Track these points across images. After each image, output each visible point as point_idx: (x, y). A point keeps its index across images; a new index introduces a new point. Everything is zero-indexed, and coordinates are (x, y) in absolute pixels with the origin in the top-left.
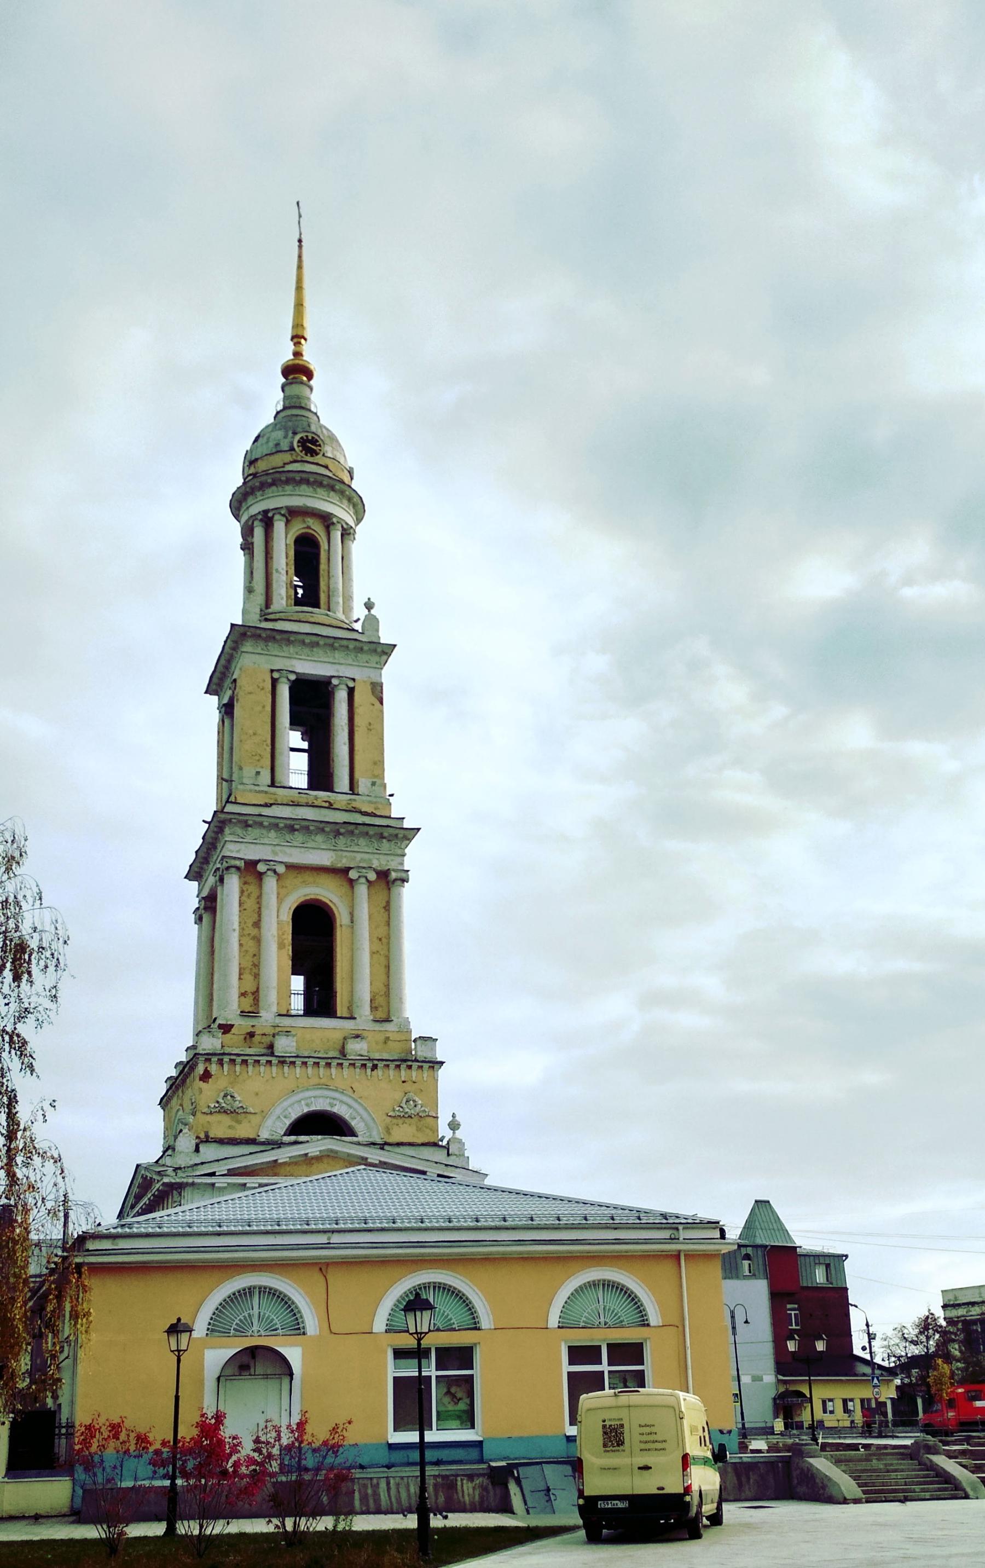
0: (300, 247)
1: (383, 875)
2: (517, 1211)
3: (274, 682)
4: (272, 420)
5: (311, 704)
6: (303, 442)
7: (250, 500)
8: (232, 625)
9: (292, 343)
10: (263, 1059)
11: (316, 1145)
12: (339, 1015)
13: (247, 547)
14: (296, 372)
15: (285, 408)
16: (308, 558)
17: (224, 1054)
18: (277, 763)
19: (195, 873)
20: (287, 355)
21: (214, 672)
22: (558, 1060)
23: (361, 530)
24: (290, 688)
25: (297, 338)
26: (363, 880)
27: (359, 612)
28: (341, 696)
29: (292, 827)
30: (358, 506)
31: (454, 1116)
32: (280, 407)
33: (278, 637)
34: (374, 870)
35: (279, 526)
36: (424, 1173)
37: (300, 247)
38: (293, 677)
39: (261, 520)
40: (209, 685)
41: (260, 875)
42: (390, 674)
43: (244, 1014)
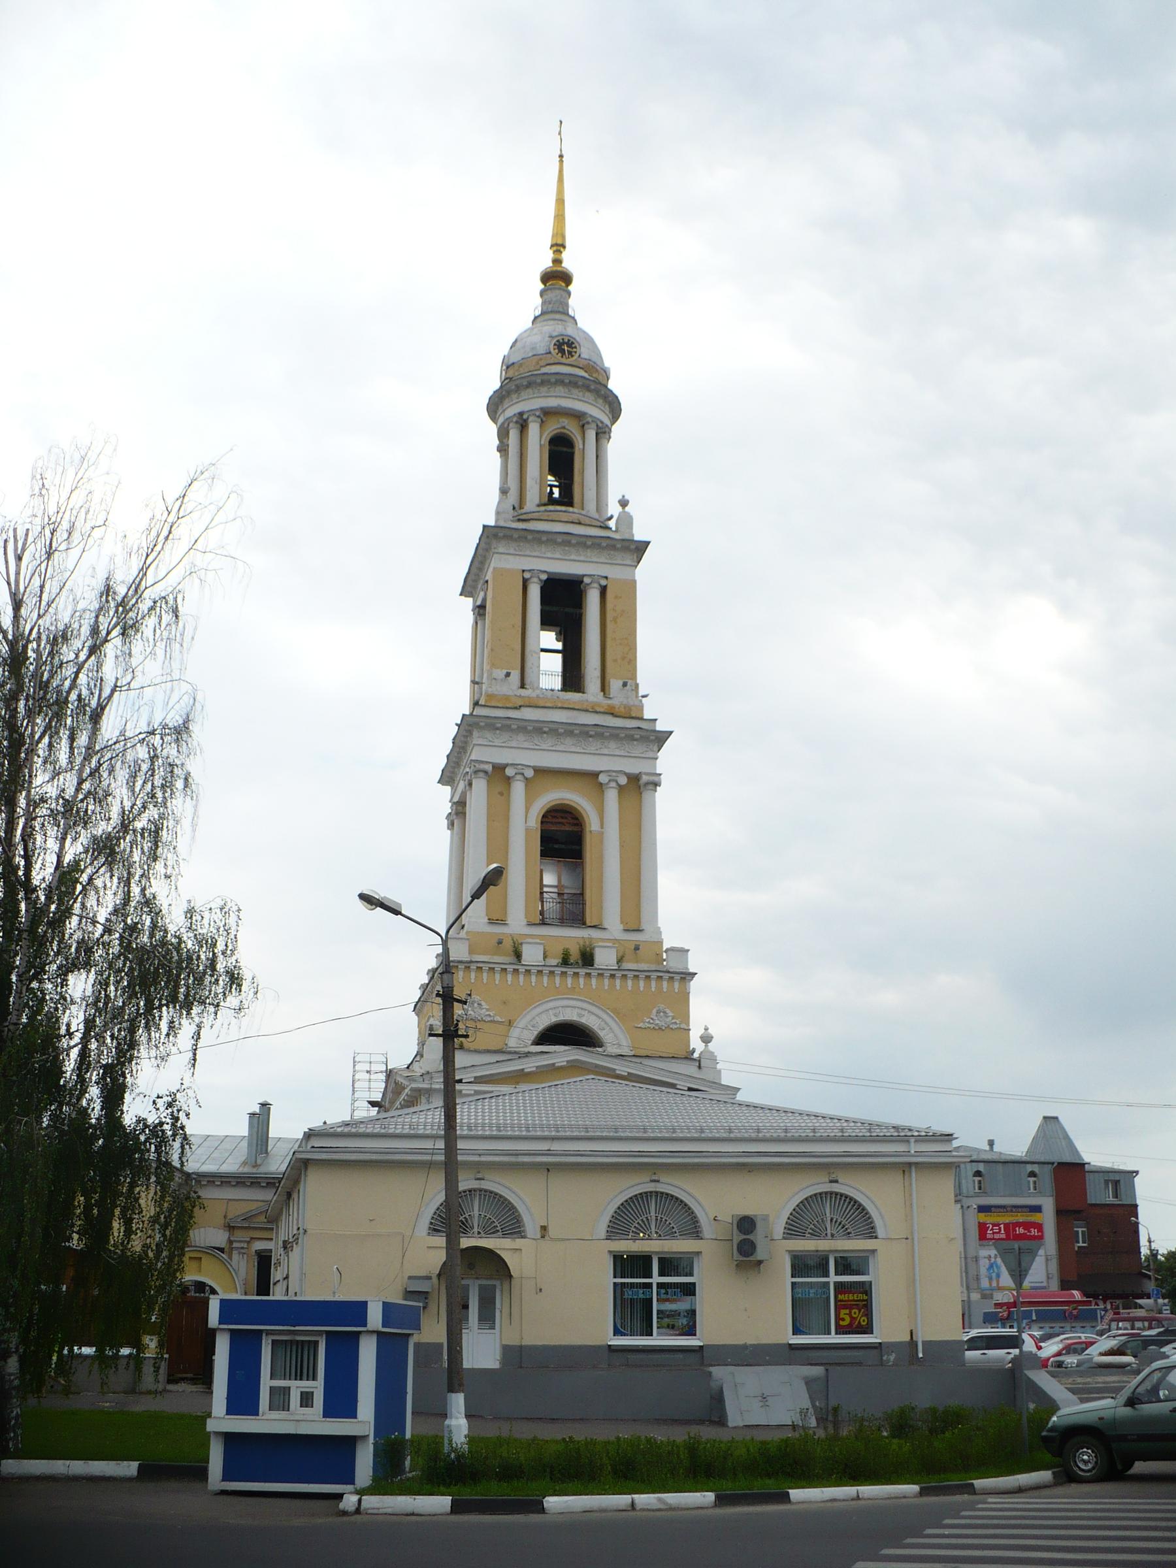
0: (561, 162)
1: (634, 779)
2: (772, 1124)
3: (525, 583)
4: (530, 325)
5: (563, 603)
6: (560, 346)
7: (506, 403)
8: (484, 526)
9: (551, 252)
11: (562, 1054)
12: (588, 923)
13: (503, 449)
14: (556, 279)
15: (542, 314)
16: (561, 457)
17: (471, 962)
18: (528, 664)
19: (447, 778)
20: (546, 263)
21: (468, 573)
22: (813, 965)
23: (616, 429)
25: (558, 246)
26: (613, 784)
27: (614, 509)
28: (592, 598)
29: (539, 730)
30: (614, 407)
31: (706, 1029)
32: (538, 312)
33: (530, 537)
34: (626, 774)
35: (534, 428)
36: (673, 1086)
37: (561, 162)
38: (544, 577)
39: (517, 422)
40: (463, 587)
41: (508, 780)
42: (645, 572)
43: (492, 922)
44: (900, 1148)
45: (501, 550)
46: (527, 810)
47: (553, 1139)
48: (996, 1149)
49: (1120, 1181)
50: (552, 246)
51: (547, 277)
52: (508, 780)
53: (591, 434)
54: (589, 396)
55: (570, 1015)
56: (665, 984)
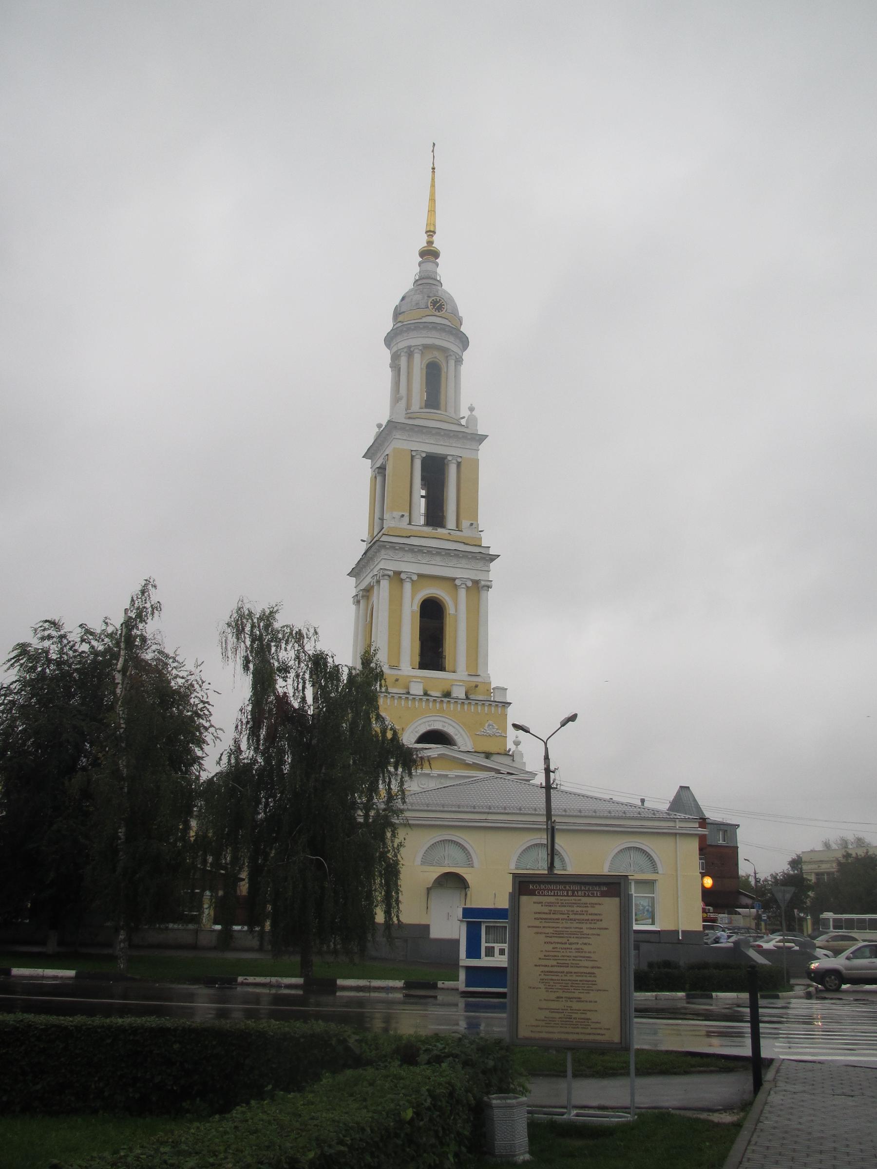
0: (433, 172)
1: (476, 582)
3: (412, 457)
6: (434, 303)
10: (404, 696)
14: (429, 254)
16: (434, 377)
20: (422, 243)
23: (466, 355)
24: (422, 461)
25: (431, 233)
26: (464, 586)
27: (464, 412)
28: (452, 470)
30: (464, 342)
32: (417, 278)
35: (417, 357)
37: (433, 172)
38: (424, 455)
41: (402, 580)
42: (484, 452)
44: (671, 824)
45: (398, 437)
46: (413, 599)
47: (488, 813)
48: (646, 804)
49: (729, 830)
50: (427, 232)
51: (423, 254)
52: (402, 580)
53: (452, 363)
54: (452, 339)
55: (438, 726)
56: (493, 709)
